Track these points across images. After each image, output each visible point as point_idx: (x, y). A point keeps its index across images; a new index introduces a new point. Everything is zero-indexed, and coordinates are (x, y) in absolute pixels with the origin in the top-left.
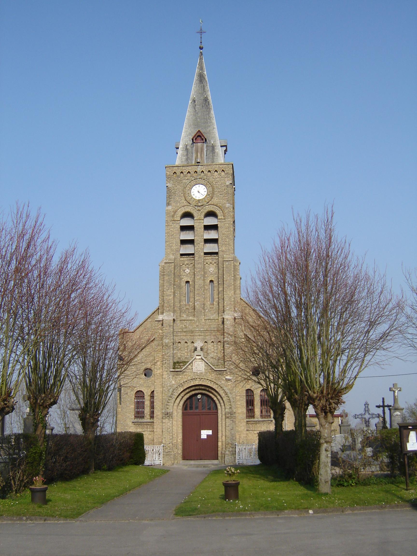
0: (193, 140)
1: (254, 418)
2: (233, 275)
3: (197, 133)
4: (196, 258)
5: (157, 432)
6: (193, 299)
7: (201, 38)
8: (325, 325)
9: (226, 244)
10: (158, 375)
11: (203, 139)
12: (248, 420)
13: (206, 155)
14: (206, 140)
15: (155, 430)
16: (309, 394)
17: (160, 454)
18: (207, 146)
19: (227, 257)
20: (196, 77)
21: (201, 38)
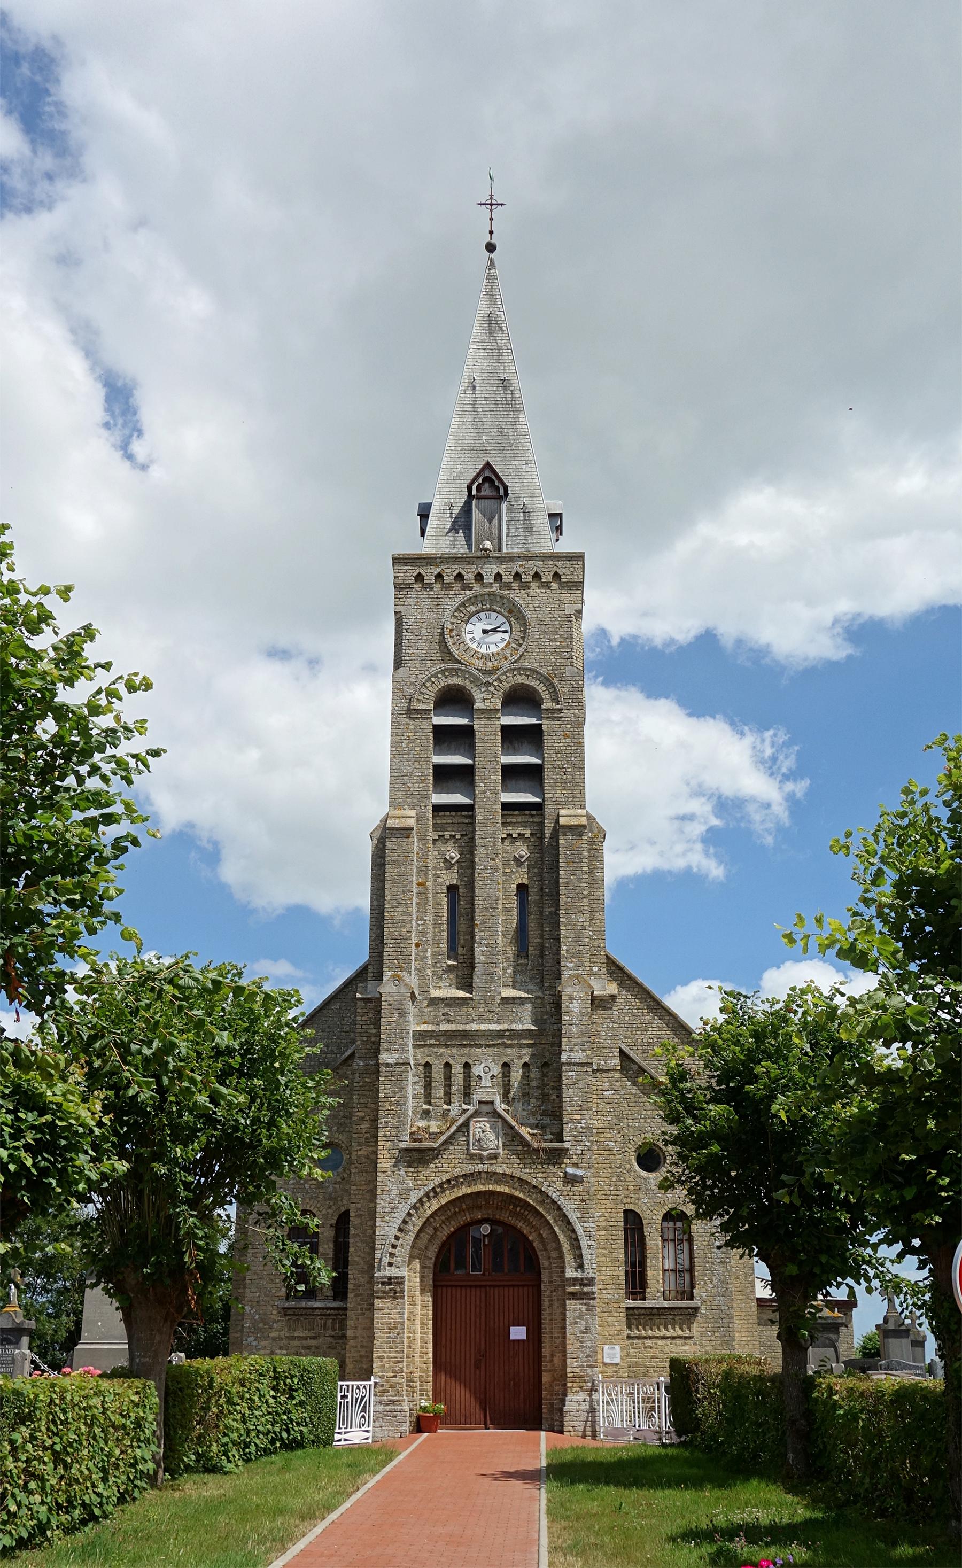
0: (469, 488)
1: (644, 1299)
2: (586, 869)
3: (482, 470)
4: (479, 818)
5: (355, 1337)
6: (468, 937)
7: (491, 219)
8: (863, 1386)
9: (564, 782)
10: (364, 1160)
11: (498, 488)
12: (631, 1303)
13: (508, 535)
14: (506, 494)
15: (349, 1333)
16: (34, 1158)
17: (364, 1410)
18: (509, 510)
19: (567, 816)
20: (477, 329)
21: (491, 219)
